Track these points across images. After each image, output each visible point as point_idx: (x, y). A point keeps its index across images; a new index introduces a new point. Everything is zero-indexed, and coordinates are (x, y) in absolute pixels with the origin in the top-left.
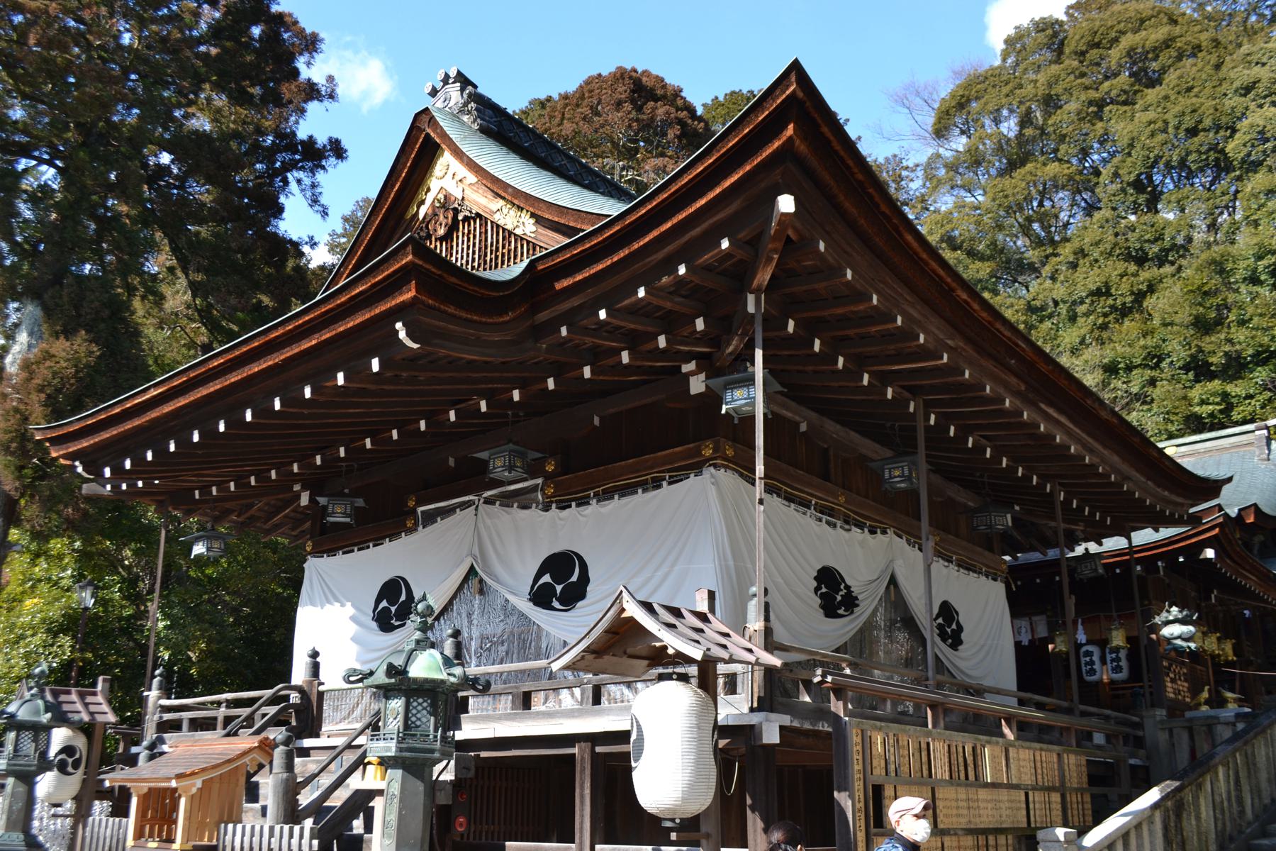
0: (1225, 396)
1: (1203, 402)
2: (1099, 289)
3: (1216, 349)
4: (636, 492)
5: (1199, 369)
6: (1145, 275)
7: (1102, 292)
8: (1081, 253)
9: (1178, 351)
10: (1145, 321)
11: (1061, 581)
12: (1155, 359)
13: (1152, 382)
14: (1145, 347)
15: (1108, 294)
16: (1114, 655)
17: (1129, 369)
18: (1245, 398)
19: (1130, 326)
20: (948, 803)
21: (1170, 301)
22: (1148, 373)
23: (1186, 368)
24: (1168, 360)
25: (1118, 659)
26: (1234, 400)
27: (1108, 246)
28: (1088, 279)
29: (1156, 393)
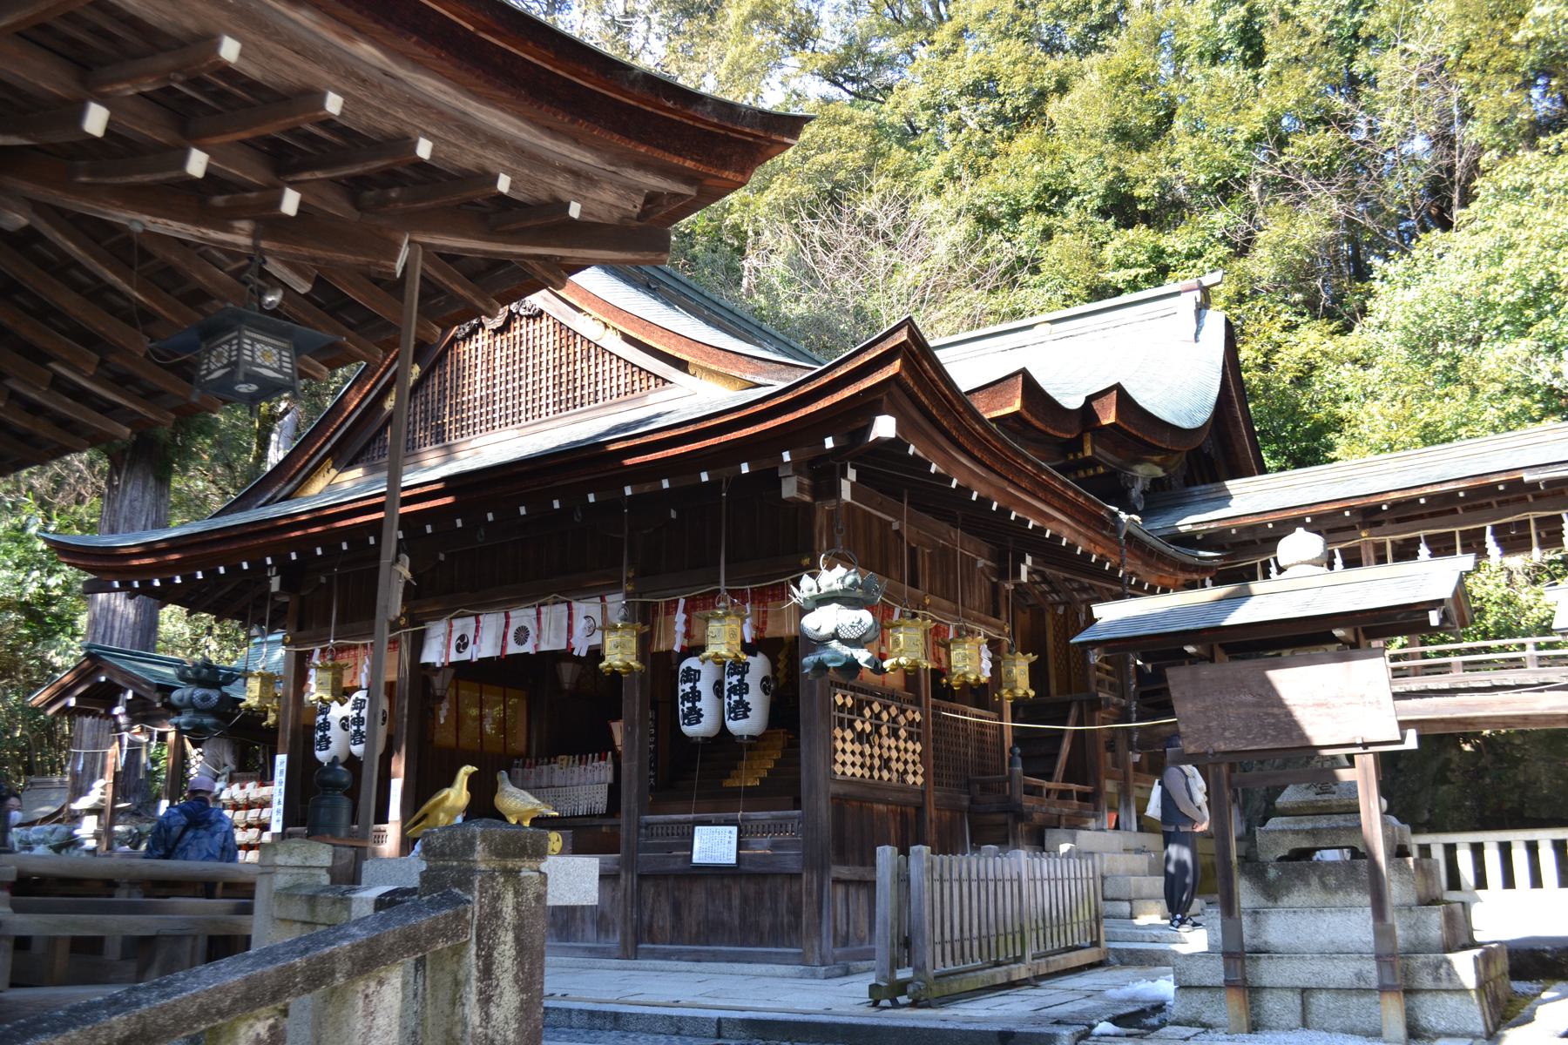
0: (1159, 253)
1: (1121, 264)
2: (977, 84)
3: (1146, 174)
4: (409, 39)
5: (1121, 208)
6: (1056, 64)
7: (979, 90)
8: (961, 33)
9: (1090, 181)
10: (1046, 138)
11: (1426, 496)
12: (1054, 197)
13: (1047, 234)
14: (1039, 177)
15: (993, 95)
16: (734, 680)
17: (1015, 215)
18: (1188, 257)
19: (1025, 142)
20: (99, 636)
21: (1087, 103)
22: (1043, 220)
23: (1103, 213)
24: (1076, 199)
25: (742, 688)
26: (1172, 261)
27: (1004, 21)
28: (970, 64)
29: (1052, 251)
